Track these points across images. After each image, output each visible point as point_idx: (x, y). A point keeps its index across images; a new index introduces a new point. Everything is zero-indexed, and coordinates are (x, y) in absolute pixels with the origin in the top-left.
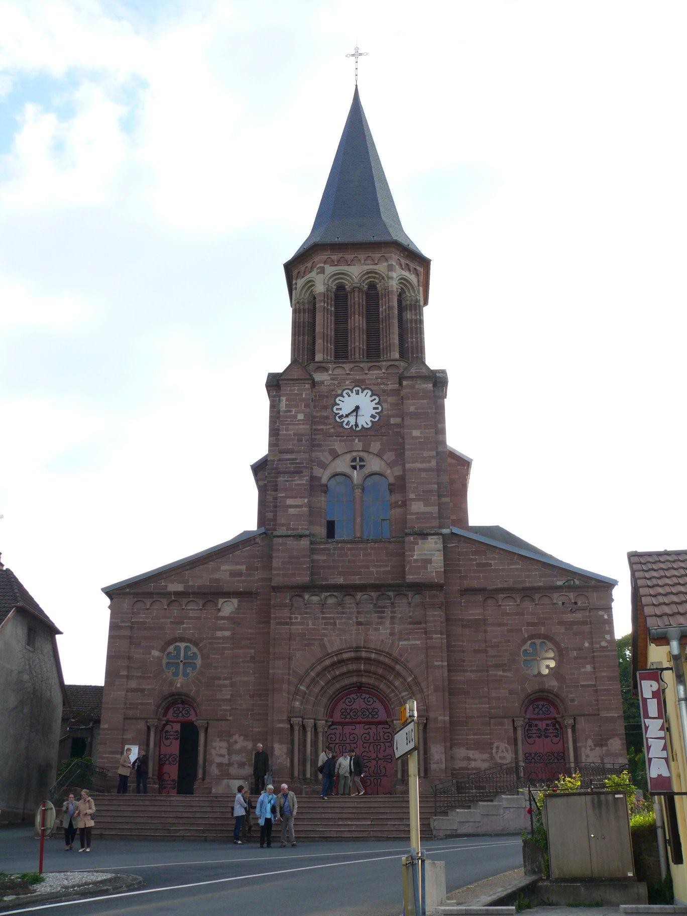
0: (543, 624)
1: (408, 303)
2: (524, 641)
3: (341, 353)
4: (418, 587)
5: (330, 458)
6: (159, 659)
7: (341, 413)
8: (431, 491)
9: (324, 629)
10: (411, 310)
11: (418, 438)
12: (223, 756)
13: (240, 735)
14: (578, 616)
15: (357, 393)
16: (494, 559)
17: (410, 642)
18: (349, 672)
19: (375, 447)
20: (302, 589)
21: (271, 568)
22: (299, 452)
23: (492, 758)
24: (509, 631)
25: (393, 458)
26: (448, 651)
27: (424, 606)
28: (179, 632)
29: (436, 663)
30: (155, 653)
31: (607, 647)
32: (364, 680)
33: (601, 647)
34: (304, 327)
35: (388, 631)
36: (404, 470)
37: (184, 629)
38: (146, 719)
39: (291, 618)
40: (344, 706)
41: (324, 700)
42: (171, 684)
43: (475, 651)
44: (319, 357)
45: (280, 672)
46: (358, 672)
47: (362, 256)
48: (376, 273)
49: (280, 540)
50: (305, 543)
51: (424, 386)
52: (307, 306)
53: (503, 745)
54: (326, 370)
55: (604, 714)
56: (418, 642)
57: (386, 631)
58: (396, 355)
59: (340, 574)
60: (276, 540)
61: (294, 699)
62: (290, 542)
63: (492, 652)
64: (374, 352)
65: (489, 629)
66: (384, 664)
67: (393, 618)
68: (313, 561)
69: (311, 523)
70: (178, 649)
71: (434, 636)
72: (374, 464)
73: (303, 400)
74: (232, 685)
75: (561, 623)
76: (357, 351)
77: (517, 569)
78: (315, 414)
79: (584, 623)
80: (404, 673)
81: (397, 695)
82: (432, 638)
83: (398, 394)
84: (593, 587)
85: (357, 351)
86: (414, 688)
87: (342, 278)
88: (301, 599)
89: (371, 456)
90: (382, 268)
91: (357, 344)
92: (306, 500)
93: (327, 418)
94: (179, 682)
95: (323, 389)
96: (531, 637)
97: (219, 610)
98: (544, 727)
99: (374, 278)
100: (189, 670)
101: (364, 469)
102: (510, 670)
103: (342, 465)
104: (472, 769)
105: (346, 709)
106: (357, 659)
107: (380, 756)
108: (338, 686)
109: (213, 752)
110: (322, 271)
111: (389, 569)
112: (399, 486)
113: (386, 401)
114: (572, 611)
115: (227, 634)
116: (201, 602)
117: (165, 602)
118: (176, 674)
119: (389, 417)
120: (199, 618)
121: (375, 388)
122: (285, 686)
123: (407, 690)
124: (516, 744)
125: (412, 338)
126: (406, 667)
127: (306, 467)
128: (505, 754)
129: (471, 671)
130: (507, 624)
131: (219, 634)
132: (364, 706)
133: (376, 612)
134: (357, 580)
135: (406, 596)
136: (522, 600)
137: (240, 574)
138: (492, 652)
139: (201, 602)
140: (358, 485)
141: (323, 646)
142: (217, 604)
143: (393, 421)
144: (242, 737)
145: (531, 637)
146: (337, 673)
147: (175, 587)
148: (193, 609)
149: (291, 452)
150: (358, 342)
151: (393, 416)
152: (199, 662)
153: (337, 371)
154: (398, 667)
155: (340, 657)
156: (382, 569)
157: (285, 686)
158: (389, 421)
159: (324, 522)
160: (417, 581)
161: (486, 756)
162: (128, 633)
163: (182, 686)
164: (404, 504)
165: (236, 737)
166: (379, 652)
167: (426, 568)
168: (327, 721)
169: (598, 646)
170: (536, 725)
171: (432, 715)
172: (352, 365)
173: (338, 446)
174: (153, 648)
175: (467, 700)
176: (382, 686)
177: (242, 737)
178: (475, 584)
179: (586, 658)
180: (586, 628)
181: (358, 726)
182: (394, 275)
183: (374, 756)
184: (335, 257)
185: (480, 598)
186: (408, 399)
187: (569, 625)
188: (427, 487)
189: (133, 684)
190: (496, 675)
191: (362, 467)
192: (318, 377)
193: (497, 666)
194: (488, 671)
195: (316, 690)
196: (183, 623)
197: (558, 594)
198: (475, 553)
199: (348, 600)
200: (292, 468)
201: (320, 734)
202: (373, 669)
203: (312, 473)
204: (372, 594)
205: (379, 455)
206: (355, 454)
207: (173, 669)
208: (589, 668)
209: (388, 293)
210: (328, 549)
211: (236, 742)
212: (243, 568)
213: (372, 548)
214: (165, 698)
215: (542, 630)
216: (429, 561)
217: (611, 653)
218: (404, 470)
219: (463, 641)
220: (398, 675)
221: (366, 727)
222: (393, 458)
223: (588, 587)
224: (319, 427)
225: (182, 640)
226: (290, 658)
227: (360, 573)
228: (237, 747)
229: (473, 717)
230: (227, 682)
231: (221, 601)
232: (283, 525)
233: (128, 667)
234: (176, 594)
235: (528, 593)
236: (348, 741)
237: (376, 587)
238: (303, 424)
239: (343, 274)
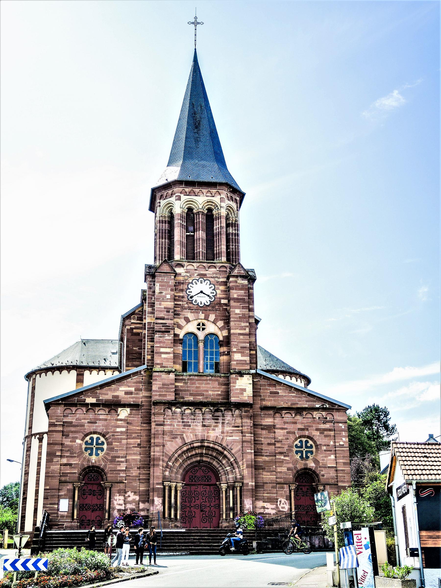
0: (307, 429)
1: (231, 222)
2: (296, 439)
3: (191, 256)
4: (240, 405)
5: (185, 323)
6: (81, 445)
7: (192, 294)
8: (246, 347)
9: (183, 429)
10: (232, 227)
11: (239, 314)
12: (121, 505)
13: (132, 492)
14: (327, 426)
15: (201, 283)
16: (280, 389)
17: (234, 438)
18: (196, 454)
19: (212, 317)
20: (170, 404)
21: (150, 390)
22: (168, 319)
23: (277, 507)
24: (288, 433)
25: (223, 325)
26: (255, 444)
27: (241, 417)
28: (93, 428)
29: (248, 451)
30: (78, 441)
31: (343, 445)
32: (204, 459)
33: (340, 445)
34: (165, 233)
35: (221, 431)
36: (229, 333)
37: (96, 426)
38: (72, 483)
39: (164, 422)
40: (191, 474)
41: (181, 471)
42: (89, 461)
43: (269, 444)
44: (177, 257)
45: (158, 454)
46: (201, 455)
47: (205, 191)
48: (212, 202)
49: (157, 374)
50: (172, 376)
51: (243, 282)
52: (167, 219)
53: (283, 500)
54: (183, 266)
55: (340, 484)
56: (238, 438)
57: (226, 432)
58: (224, 259)
59: (191, 395)
60: (154, 374)
61: (166, 471)
62: (164, 376)
63: (278, 445)
64: (211, 255)
65: (276, 431)
66: (217, 450)
67: (223, 423)
68: (176, 386)
69: (174, 363)
70: (92, 439)
71: (247, 435)
72: (211, 328)
73: (170, 286)
74: (127, 461)
75: (317, 430)
76: (201, 254)
77: (293, 397)
78: (176, 294)
79: (330, 430)
80: (229, 456)
81: (223, 469)
82: (245, 436)
83: (226, 285)
84: (336, 409)
85: (201, 254)
86: (235, 465)
87: (191, 204)
88: (170, 411)
89: (209, 323)
90: (217, 199)
91: (201, 250)
92: (172, 349)
93: (183, 297)
94: (94, 458)
95: (180, 278)
96: (300, 437)
97: (118, 415)
98: (306, 490)
99: (211, 205)
100: (99, 452)
101: (205, 331)
102: (288, 456)
103: (192, 327)
104: (266, 514)
105: (192, 476)
106: (202, 447)
107: (212, 505)
108: (189, 462)
109: (115, 502)
110: (179, 199)
111: (220, 393)
112: (227, 342)
113: (218, 289)
114: (324, 423)
115: (124, 429)
116: (107, 410)
117: (84, 409)
118: (91, 454)
119: (220, 299)
120: (106, 420)
121: (212, 280)
122: (161, 463)
123: (229, 466)
124: (290, 500)
125: (233, 246)
126: (230, 452)
127: (172, 329)
128: (285, 505)
129: (266, 456)
130: (286, 429)
131: (118, 430)
132: (203, 474)
133: (213, 419)
134: (200, 399)
135: (231, 410)
136: (296, 415)
137: (131, 393)
138: (278, 445)
139: (107, 410)
140: (202, 340)
141: (183, 439)
142: (117, 412)
143: (223, 301)
144: (133, 493)
145: (300, 437)
146: (190, 455)
147: (90, 400)
148: (102, 413)
149: (163, 319)
150: (201, 248)
151: (223, 299)
152: (105, 447)
153: (190, 267)
154: (225, 452)
155: (192, 446)
156: (216, 393)
157: (161, 463)
158: (220, 301)
159: (181, 361)
160: (238, 401)
161: (274, 506)
162: (61, 429)
163: (95, 461)
164: (228, 354)
165: (129, 493)
166: (215, 443)
167: (242, 394)
168: (182, 484)
169: (338, 444)
170: (302, 489)
171: (245, 481)
172: (198, 264)
173: (190, 316)
174: (77, 438)
175: (264, 473)
176: (215, 463)
177: (133, 493)
178: (269, 404)
179: (331, 451)
180: (332, 433)
181: (199, 486)
182: (223, 204)
183: (212, 505)
184: (187, 190)
185: (271, 412)
186: (233, 290)
187: (322, 431)
188: (244, 345)
189: (64, 461)
190: (280, 459)
191: (203, 329)
192: (178, 270)
193: (281, 453)
194: (275, 456)
195: (177, 465)
196: (96, 423)
197: (316, 412)
198: (270, 385)
199: (197, 411)
200: (163, 329)
201: (179, 492)
202: (210, 453)
203: (174, 332)
204: (212, 408)
205: (214, 322)
206: (199, 321)
207: (89, 451)
208: (333, 457)
209: (219, 217)
210: (185, 380)
211: (129, 496)
212: (133, 389)
213: (210, 380)
214: (85, 469)
215: (307, 433)
216: (244, 390)
217: (345, 449)
218: (229, 333)
219: (262, 438)
220: (225, 457)
221: (204, 487)
222: (223, 325)
223: (333, 409)
224: (178, 303)
225: (95, 433)
226: (164, 446)
227: (203, 395)
228: (130, 499)
229: (267, 483)
230: (123, 460)
231: (120, 409)
232: (158, 364)
233: (61, 450)
234: (92, 404)
235: (299, 411)
236: (193, 495)
237: (213, 404)
238: (170, 302)
239: (192, 201)
